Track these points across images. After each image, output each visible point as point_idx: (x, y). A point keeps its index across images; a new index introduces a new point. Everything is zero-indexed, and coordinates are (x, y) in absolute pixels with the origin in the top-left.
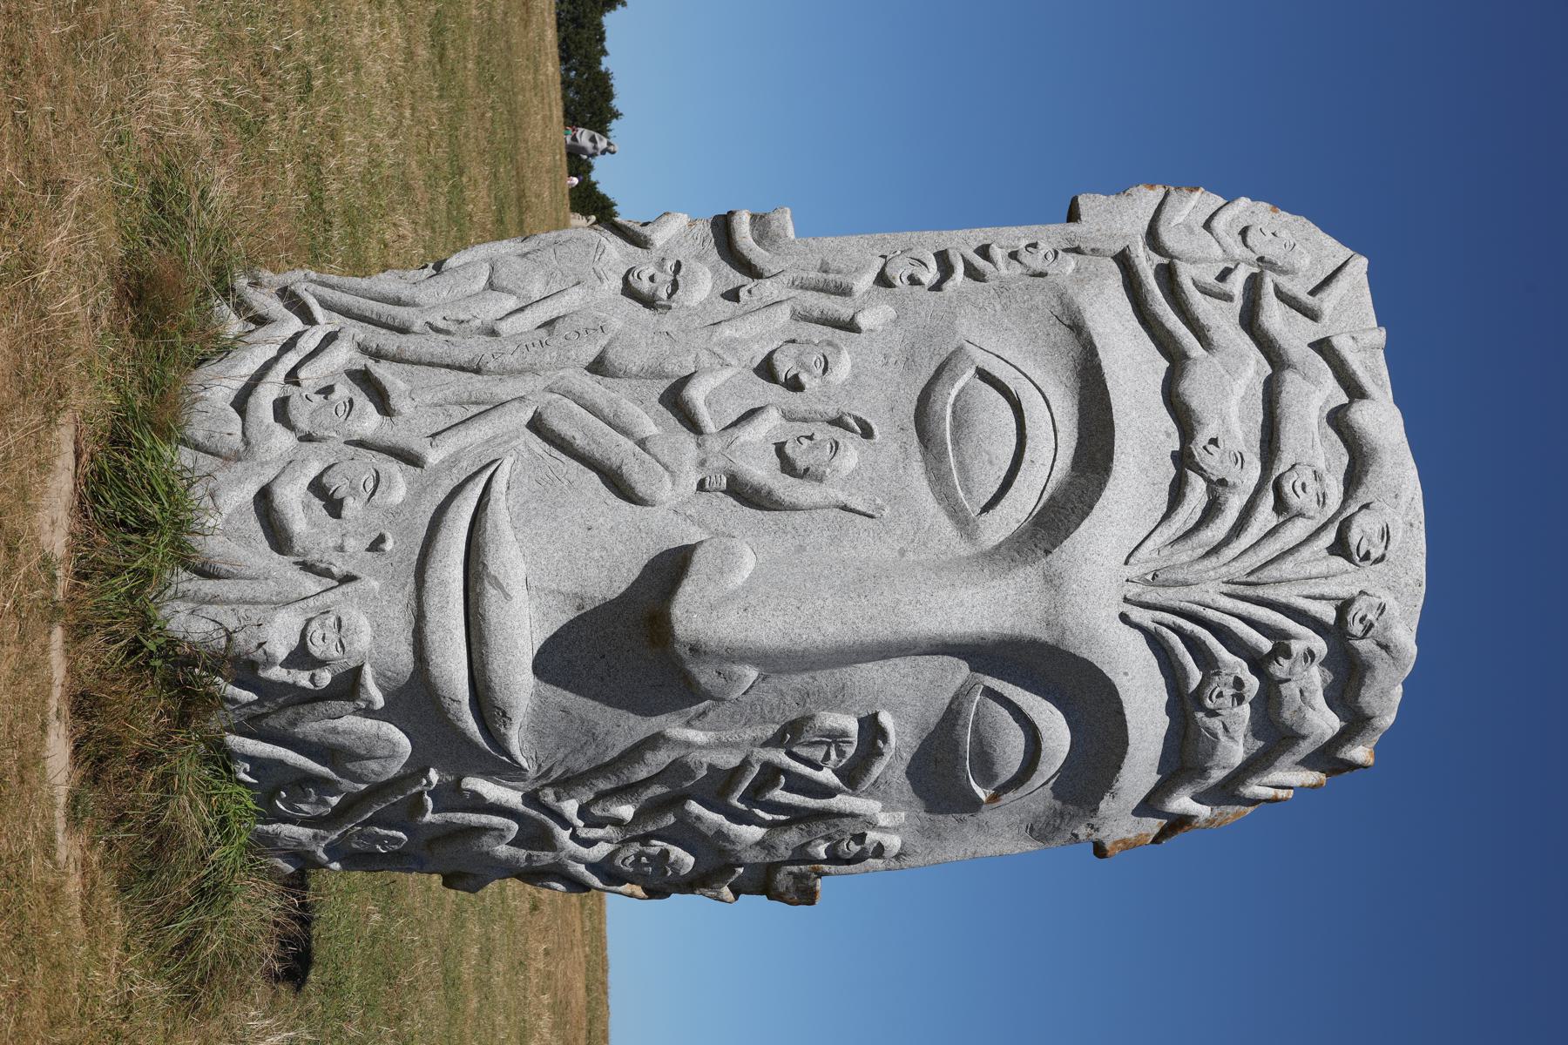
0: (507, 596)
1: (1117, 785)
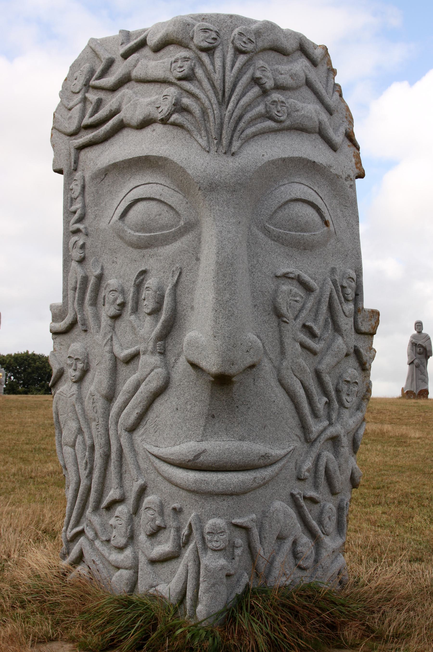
0: (204, 451)
1: (324, 164)
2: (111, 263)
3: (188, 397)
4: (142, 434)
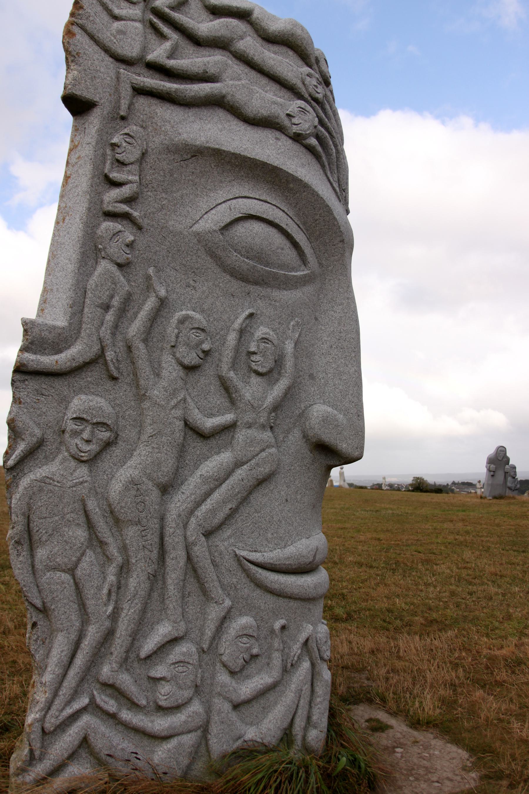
2: (184, 286)
3: (299, 485)
4: (229, 537)
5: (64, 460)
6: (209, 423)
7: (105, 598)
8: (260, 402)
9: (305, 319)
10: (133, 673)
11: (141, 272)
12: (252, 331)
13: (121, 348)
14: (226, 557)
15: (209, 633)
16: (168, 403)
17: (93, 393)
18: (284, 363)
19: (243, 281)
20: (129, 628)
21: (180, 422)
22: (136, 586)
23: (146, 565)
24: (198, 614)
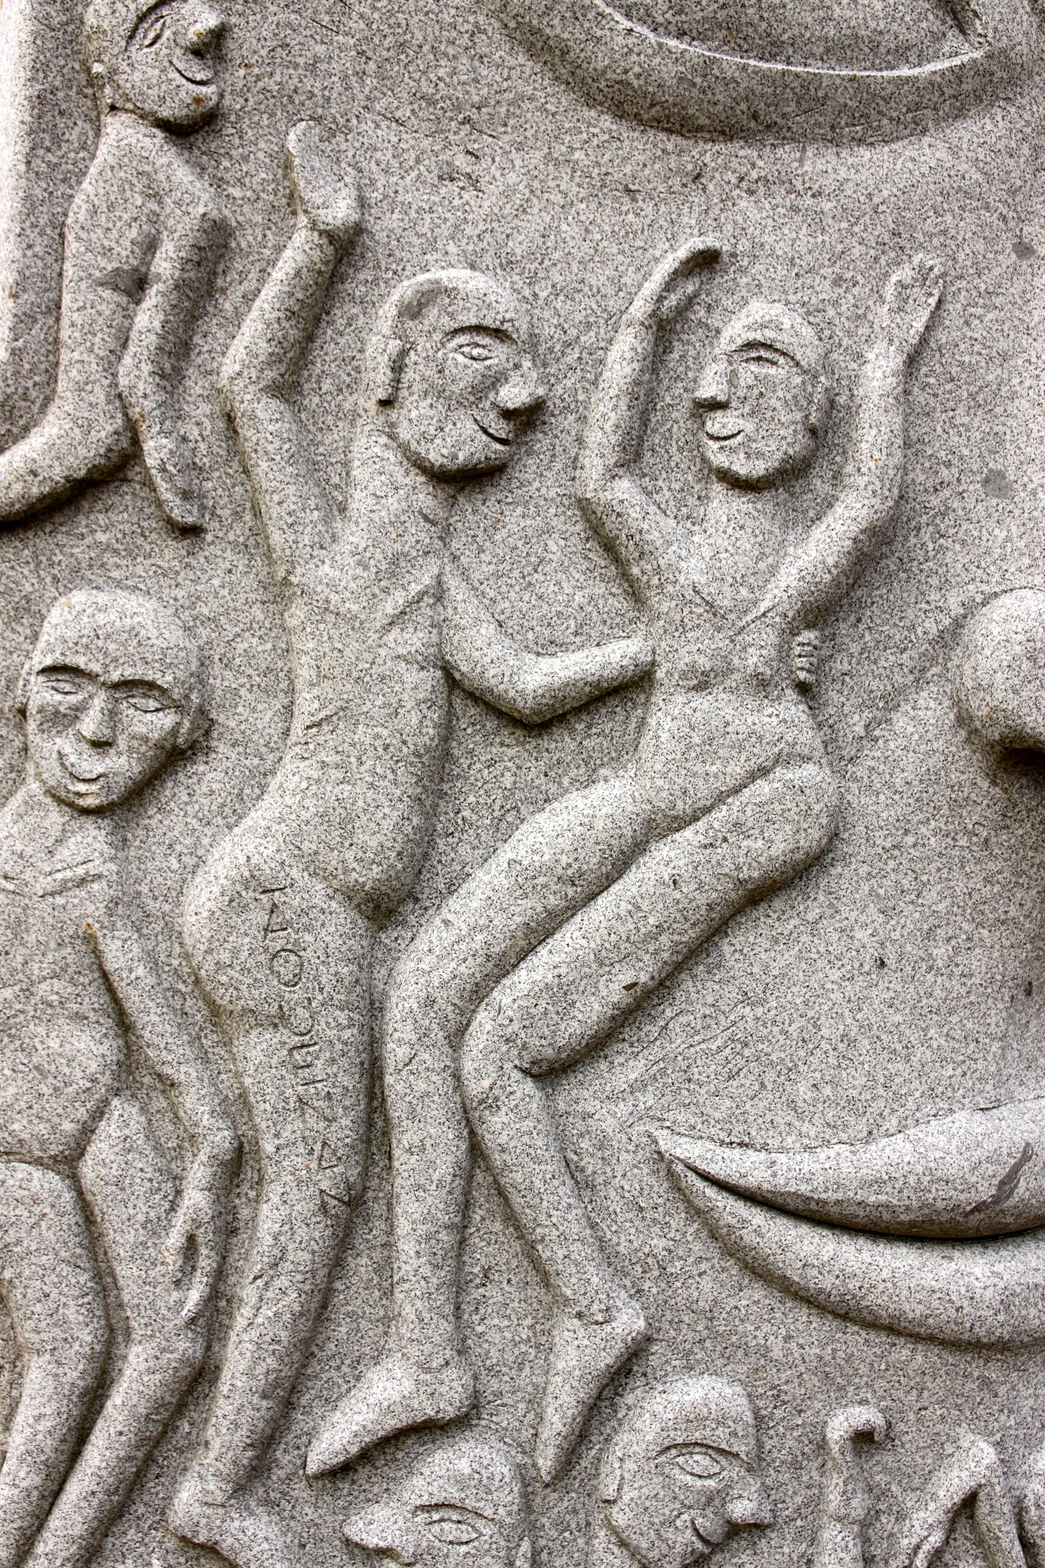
3: (941, 907)
5: (30, 804)
6: (534, 676)
7: (173, 1261)
8: (744, 592)
9: (961, 256)
10: (293, 1518)
11: (262, 145)
12: (715, 321)
13: (207, 422)
14: (624, 1156)
15: (558, 1417)
16: (371, 608)
17: (119, 584)
18: (854, 435)
19: (670, 131)
20: (260, 1370)
21: (423, 674)
22: (280, 1233)
23: (314, 1165)
24: (523, 1348)
